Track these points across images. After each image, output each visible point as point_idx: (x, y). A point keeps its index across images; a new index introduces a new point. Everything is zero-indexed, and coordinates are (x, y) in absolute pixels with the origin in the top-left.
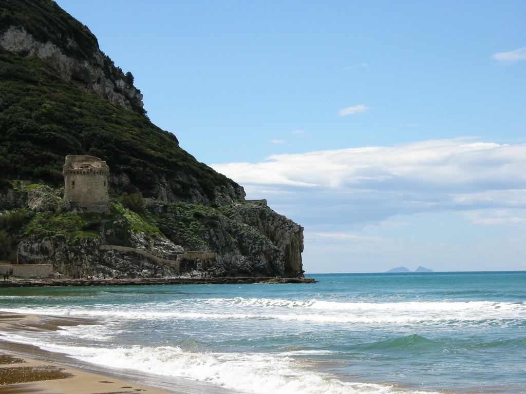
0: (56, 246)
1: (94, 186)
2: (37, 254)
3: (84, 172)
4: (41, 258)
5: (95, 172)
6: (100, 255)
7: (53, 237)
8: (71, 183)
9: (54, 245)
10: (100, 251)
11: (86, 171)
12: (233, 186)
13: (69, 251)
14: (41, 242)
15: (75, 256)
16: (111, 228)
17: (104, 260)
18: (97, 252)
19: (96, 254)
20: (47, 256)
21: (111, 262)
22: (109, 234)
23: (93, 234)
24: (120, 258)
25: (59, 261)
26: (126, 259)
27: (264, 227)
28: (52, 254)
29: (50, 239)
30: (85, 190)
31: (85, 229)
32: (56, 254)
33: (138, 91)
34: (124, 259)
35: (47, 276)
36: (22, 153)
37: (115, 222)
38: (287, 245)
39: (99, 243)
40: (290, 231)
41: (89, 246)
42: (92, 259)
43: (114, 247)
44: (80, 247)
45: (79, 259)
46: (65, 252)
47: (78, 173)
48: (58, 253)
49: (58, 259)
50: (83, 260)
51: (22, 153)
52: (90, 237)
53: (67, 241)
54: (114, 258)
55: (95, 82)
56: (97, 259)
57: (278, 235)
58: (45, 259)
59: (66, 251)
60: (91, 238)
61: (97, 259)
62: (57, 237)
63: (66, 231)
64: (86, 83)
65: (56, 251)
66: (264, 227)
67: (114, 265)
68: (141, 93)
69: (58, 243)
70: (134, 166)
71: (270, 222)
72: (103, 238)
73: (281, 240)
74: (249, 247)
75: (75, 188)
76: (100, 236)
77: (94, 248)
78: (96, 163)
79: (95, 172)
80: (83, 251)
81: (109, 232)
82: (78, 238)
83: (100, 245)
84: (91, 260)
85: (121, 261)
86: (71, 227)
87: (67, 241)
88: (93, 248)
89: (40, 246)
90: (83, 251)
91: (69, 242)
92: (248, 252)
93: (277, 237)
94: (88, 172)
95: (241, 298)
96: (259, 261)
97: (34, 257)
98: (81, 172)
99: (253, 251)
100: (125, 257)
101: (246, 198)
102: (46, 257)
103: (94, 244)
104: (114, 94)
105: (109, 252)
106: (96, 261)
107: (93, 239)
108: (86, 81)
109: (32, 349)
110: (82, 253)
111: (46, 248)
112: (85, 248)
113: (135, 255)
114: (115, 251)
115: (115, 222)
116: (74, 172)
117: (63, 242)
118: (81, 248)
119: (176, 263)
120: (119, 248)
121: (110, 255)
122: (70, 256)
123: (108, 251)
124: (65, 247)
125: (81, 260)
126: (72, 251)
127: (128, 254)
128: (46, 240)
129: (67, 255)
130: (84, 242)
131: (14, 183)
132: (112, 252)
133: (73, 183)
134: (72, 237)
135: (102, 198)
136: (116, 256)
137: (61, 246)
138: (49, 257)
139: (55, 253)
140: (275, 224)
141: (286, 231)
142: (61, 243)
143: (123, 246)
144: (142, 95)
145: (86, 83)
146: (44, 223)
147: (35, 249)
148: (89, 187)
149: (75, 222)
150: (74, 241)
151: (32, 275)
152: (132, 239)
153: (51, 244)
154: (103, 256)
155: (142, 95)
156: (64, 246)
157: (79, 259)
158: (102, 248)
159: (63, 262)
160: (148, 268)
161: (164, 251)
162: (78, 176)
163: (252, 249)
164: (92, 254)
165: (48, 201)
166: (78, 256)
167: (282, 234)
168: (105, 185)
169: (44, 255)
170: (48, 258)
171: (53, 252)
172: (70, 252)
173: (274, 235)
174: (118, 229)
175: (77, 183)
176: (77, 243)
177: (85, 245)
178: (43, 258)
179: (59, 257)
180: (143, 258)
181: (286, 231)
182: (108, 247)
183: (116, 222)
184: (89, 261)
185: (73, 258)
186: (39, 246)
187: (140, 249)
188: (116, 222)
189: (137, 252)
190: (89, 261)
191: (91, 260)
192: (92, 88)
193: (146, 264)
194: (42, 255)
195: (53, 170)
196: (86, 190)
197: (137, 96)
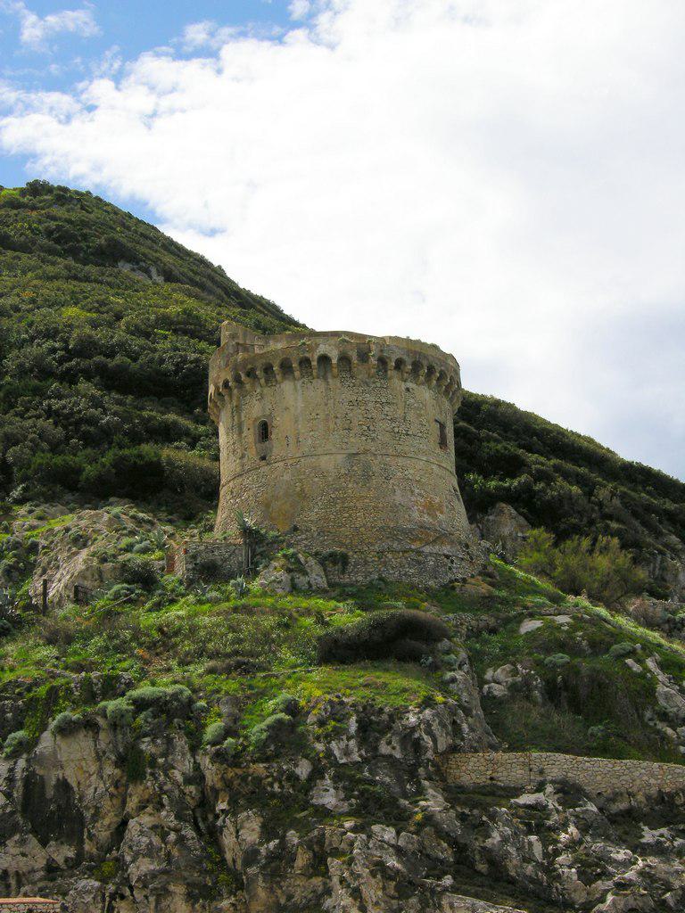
0: (132, 765)
1: (387, 438)
3: (324, 359)
4: (23, 864)
5: (382, 361)
6: (457, 828)
7: (111, 705)
8: (250, 435)
9: (121, 762)
10: (455, 794)
13: (222, 806)
14: (25, 747)
15: (268, 832)
16: (507, 655)
17: (495, 862)
18: (434, 802)
19: (429, 819)
20: (70, 852)
21: (549, 869)
22: (498, 690)
23: (402, 682)
24: (621, 841)
25: (144, 882)
26: (658, 849)
28: (102, 830)
29: (89, 725)
30: (331, 462)
31: (338, 651)
34: (643, 850)
36: (49, 413)
37: (529, 626)
39: (443, 742)
41: (373, 758)
42: (399, 851)
43: (560, 765)
44: (303, 769)
45: (302, 860)
46: (201, 814)
47: (286, 368)
48: (146, 820)
49: (145, 866)
50: (334, 864)
51: (49, 413)
52: (380, 701)
53: (213, 728)
54: (572, 845)
56: (445, 852)
58: (51, 870)
59: (205, 803)
60: (385, 702)
61: (445, 852)
62: (140, 705)
63: (211, 671)
65: (132, 803)
67: (580, 897)
69: (146, 746)
70: (541, 476)
72: (467, 712)
76: (446, 693)
77: (413, 774)
79: (382, 361)
80: (328, 796)
81: (499, 679)
82: (292, 708)
83: (454, 749)
84: (393, 862)
85: (628, 864)
86: (247, 646)
87: (213, 728)
88: (408, 771)
89: (18, 775)
90: (328, 796)
91: (228, 732)
98: (305, 362)
100: (649, 836)
102: (66, 852)
103: (411, 742)
105: (526, 799)
106: (438, 869)
107: (399, 713)
109: (644, 483)
110: (324, 813)
111: (64, 786)
112: (346, 778)
114: (569, 793)
115: (529, 626)
116: (268, 369)
117: (181, 742)
118: (317, 773)
120: (596, 772)
121: (535, 820)
122: (228, 840)
123: (518, 791)
124: (197, 777)
125: (318, 865)
126: (250, 795)
128: (66, 730)
129: (212, 836)
130: (337, 734)
131: (210, 783)
132: (548, 798)
133: (264, 431)
134: (243, 705)
135: (431, 508)
136: (584, 829)
137: (167, 768)
138: (80, 855)
139: (124, 824)
142: (169, 741)
143: (619, 755)
146: (69, 640)
148: (356, 444)
149: (269, 621)
150: (257, 730)
152: (664, 716)
153: (99, 757)
154: (483, 829)
156: (187, 766)
157: (302, 860)
158: (472, 770)
159: (179, 889)
162: (287, 386)
164: (399, 819)
165: (129, 548)
166: (293, 837)
168: (443, 443)
169: (44, 843)
170: (73, 864)
171: (110, 819)
172: (234, 810)
174: (561, 658)
175: (282, 426)
176: (287, 737)
177: (346, 750)
178: (41, 863)
179: (150, 852)
182: (510, 767)
183: (537, 624)
184: (379, 868)
185: (251, 856)
186: (10, 780)
188: (537, 624)
190: (379, 868)
191: (393, 862)
194: (33, 841)
195: (176, 455)
196: (340, 458)
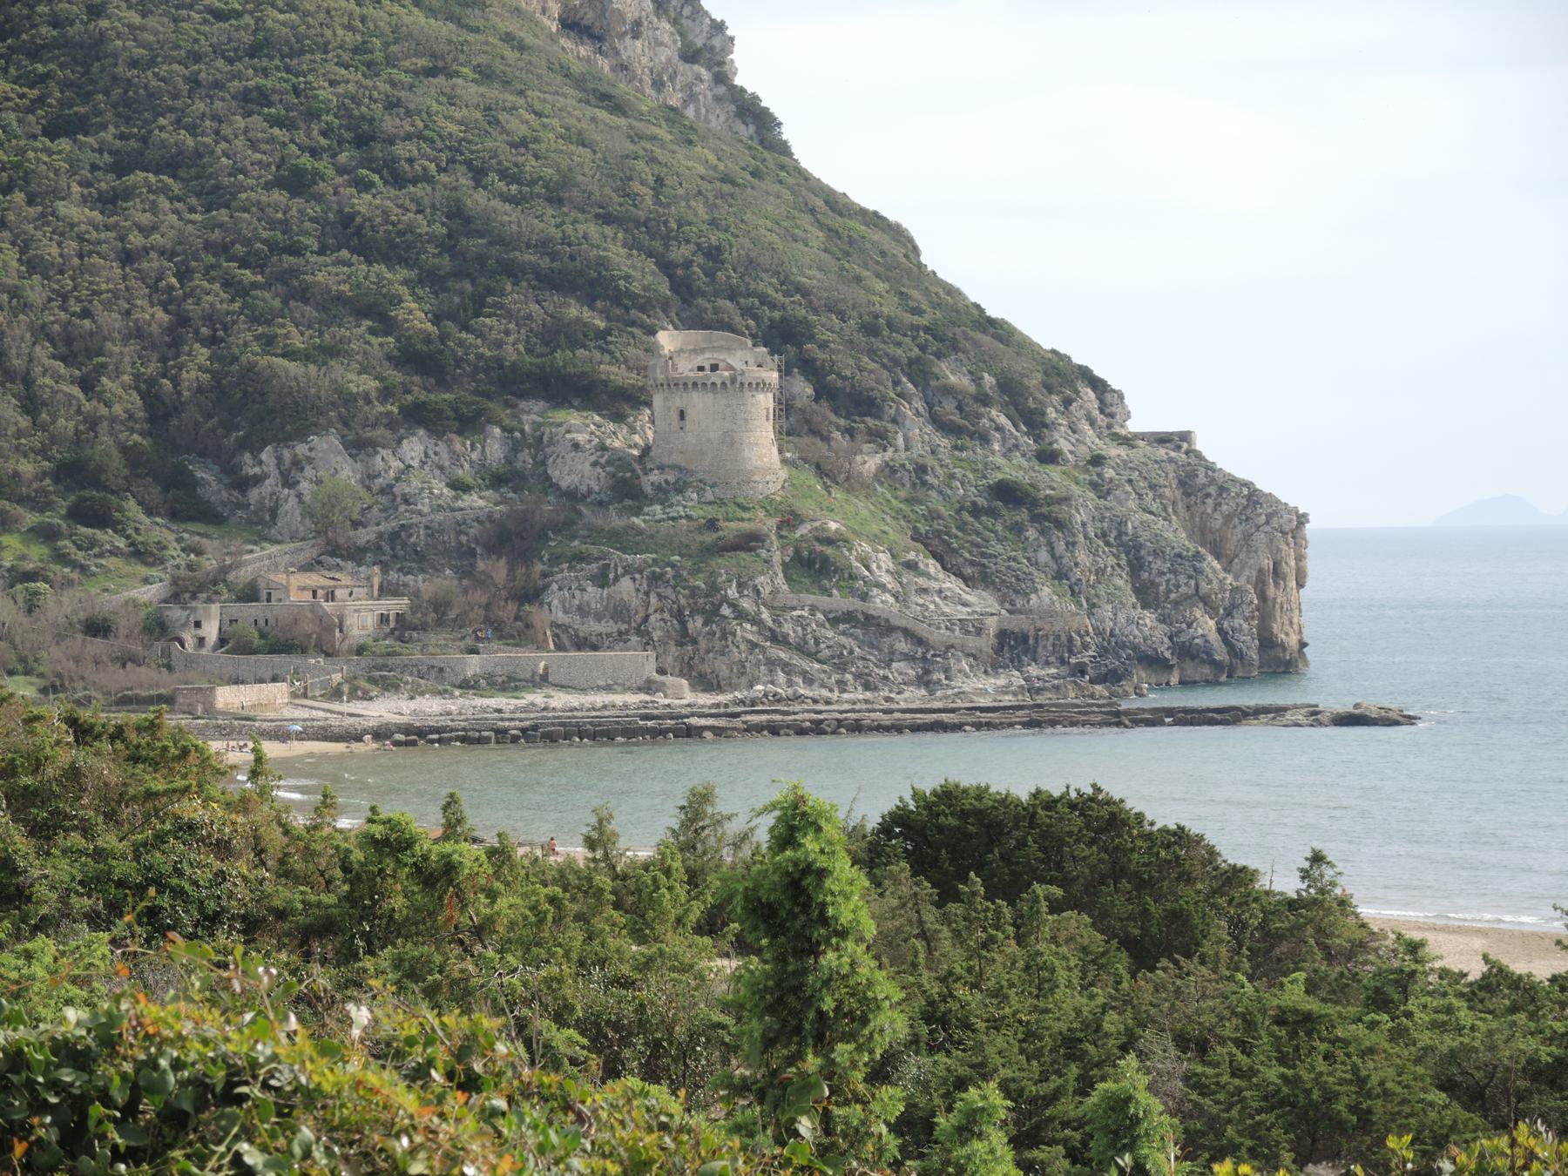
2: (599, 618)
4: (609, 630)
8: (675, 415)
11: (719, 383)
12: (1094, 389)
15: (705, 624)
17: (786, 636)
27: (1192, 516)
28: (639, 618)
32: (652, 618)
33: (719, 27)
35: (640, 683)
38: (1261, 571)
40: (1267, 528)
55: (625, 33)
57: (1235, 536)
64: (600, 39)
66: (1192, 516)
68: (729, 32)
71: (1209, 501)
73: (1242, 556)
74: (1159, 585)
75: (688, 427)
78: (739, 353)
92: (1157, 598)
93: (1230, 547)
94: (724, 384)
95: (425, 349)
96: (1189, 626)
97: (593, 627)
98: (704, 385)
99: (1173, 596)
101: (1134, 425)
104: (683, 67)
108: (596, 31)
110: (725, 617)
113: (869, 621)
119: (987, 643)
122: (690, 625)
127: (849, 617)
129: (683, 623)
133: (682, 415)
139: (647, 616)
140: (1224, 507)
141: (1258, 527)
144: (732, 39)
145: (600, 39)
147: (593, 605)
151: (601, 683)
155: (732, 39)
160: (907, 657)
161: (946, 610)
162: (694, 394)
163: (1169, 591)
167: (1247, 537)
171: (641, 614)
172: (692, 615)
173: (1223, 540)
175: (691, 415)
180: (889, 629)
181: (1258, 527)
187: (882, 603)
189: (871, 612)
192: (617, 53)
193: (902, 646)
197: (717, 42)
